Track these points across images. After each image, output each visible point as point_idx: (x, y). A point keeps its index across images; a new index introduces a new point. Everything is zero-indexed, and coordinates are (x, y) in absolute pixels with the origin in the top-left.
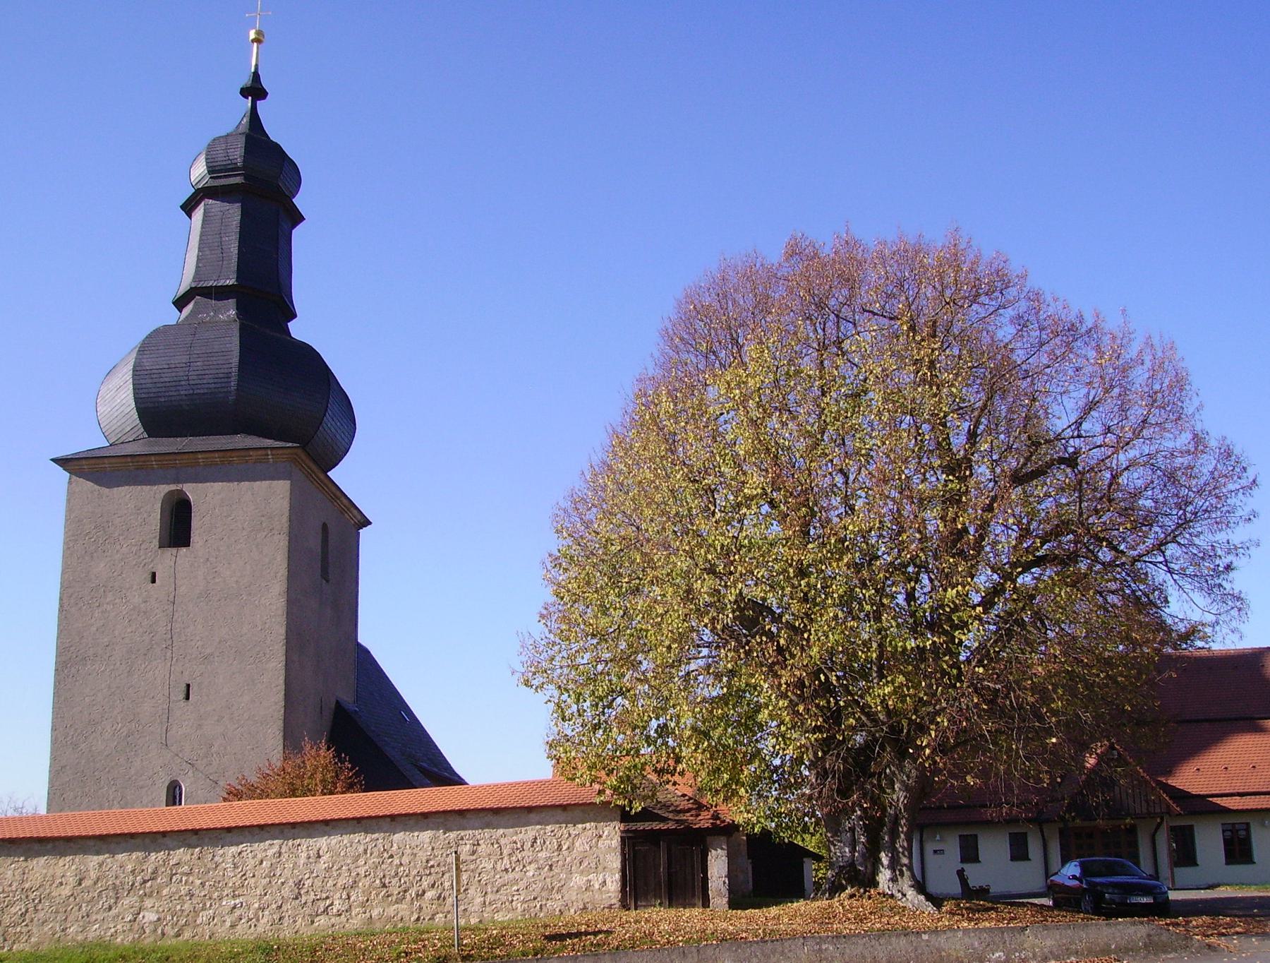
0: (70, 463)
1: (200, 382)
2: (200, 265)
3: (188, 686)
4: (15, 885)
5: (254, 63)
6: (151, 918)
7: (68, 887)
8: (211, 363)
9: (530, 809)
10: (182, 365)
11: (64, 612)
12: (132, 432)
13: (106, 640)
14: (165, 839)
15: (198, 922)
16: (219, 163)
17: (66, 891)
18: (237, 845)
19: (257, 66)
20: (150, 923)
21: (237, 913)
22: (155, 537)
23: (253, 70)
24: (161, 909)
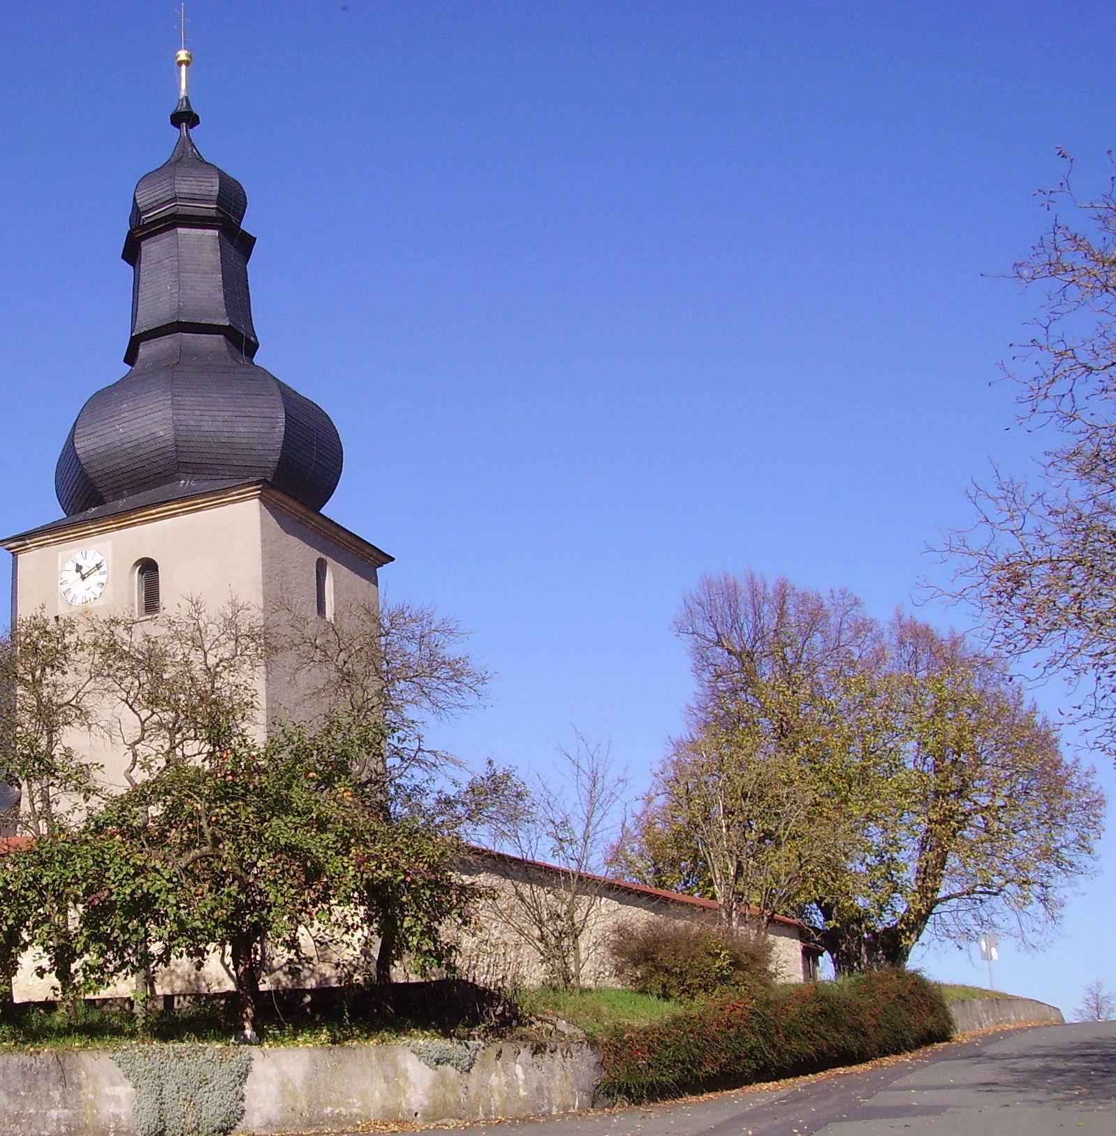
23: (183, 94)
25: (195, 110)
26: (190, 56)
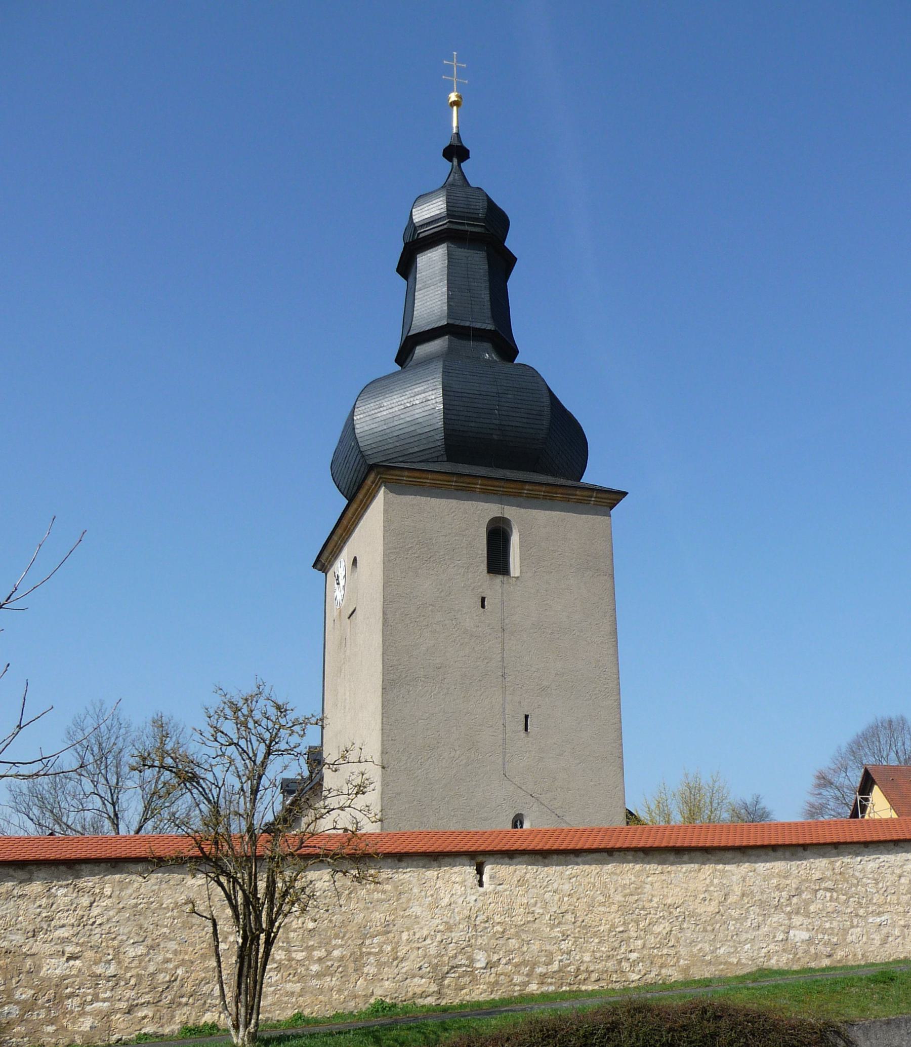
0: (392, 472)
1: (514, 414)
2: (452, 304)
3: (527, 717)
4: (655, 900)
5: (455, 124)
6: (803, 937)
7: (713, 903)
8: (486, 402)
9: (805, 847)
10: (492, 394)
11: (389, 628)
12: (419, 454)
13: (438, 661)
14: (806, 853)
15: (849, 940)
16: (459, 209)
17: (712, 908)
18: (801, 861)
19: (458, 127)
20: (803, 942)
21: (884, 930)
22: (483, 562)
23: (455, 131)
24: (810, 927)
25: (466, 144)
26: (459, 97)
